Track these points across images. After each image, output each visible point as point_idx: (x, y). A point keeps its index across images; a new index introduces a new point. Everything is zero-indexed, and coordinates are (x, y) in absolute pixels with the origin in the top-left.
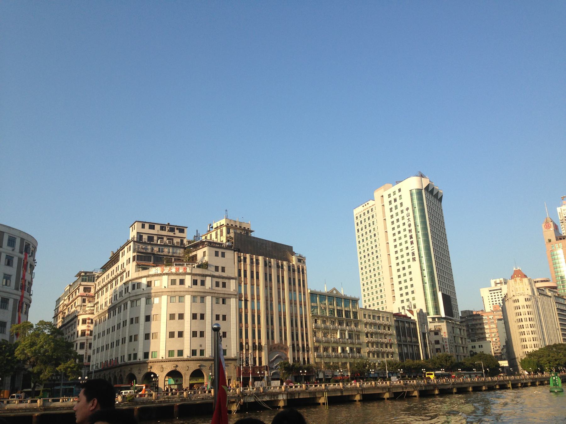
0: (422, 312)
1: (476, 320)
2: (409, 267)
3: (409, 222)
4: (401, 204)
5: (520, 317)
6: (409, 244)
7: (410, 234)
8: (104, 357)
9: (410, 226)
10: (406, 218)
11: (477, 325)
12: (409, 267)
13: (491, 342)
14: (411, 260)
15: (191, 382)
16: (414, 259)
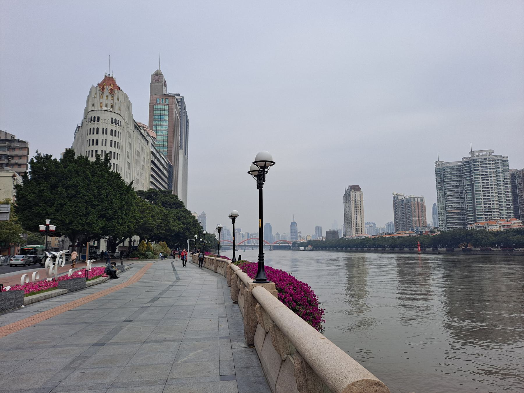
1: (14, 149)
11: (13, 157)
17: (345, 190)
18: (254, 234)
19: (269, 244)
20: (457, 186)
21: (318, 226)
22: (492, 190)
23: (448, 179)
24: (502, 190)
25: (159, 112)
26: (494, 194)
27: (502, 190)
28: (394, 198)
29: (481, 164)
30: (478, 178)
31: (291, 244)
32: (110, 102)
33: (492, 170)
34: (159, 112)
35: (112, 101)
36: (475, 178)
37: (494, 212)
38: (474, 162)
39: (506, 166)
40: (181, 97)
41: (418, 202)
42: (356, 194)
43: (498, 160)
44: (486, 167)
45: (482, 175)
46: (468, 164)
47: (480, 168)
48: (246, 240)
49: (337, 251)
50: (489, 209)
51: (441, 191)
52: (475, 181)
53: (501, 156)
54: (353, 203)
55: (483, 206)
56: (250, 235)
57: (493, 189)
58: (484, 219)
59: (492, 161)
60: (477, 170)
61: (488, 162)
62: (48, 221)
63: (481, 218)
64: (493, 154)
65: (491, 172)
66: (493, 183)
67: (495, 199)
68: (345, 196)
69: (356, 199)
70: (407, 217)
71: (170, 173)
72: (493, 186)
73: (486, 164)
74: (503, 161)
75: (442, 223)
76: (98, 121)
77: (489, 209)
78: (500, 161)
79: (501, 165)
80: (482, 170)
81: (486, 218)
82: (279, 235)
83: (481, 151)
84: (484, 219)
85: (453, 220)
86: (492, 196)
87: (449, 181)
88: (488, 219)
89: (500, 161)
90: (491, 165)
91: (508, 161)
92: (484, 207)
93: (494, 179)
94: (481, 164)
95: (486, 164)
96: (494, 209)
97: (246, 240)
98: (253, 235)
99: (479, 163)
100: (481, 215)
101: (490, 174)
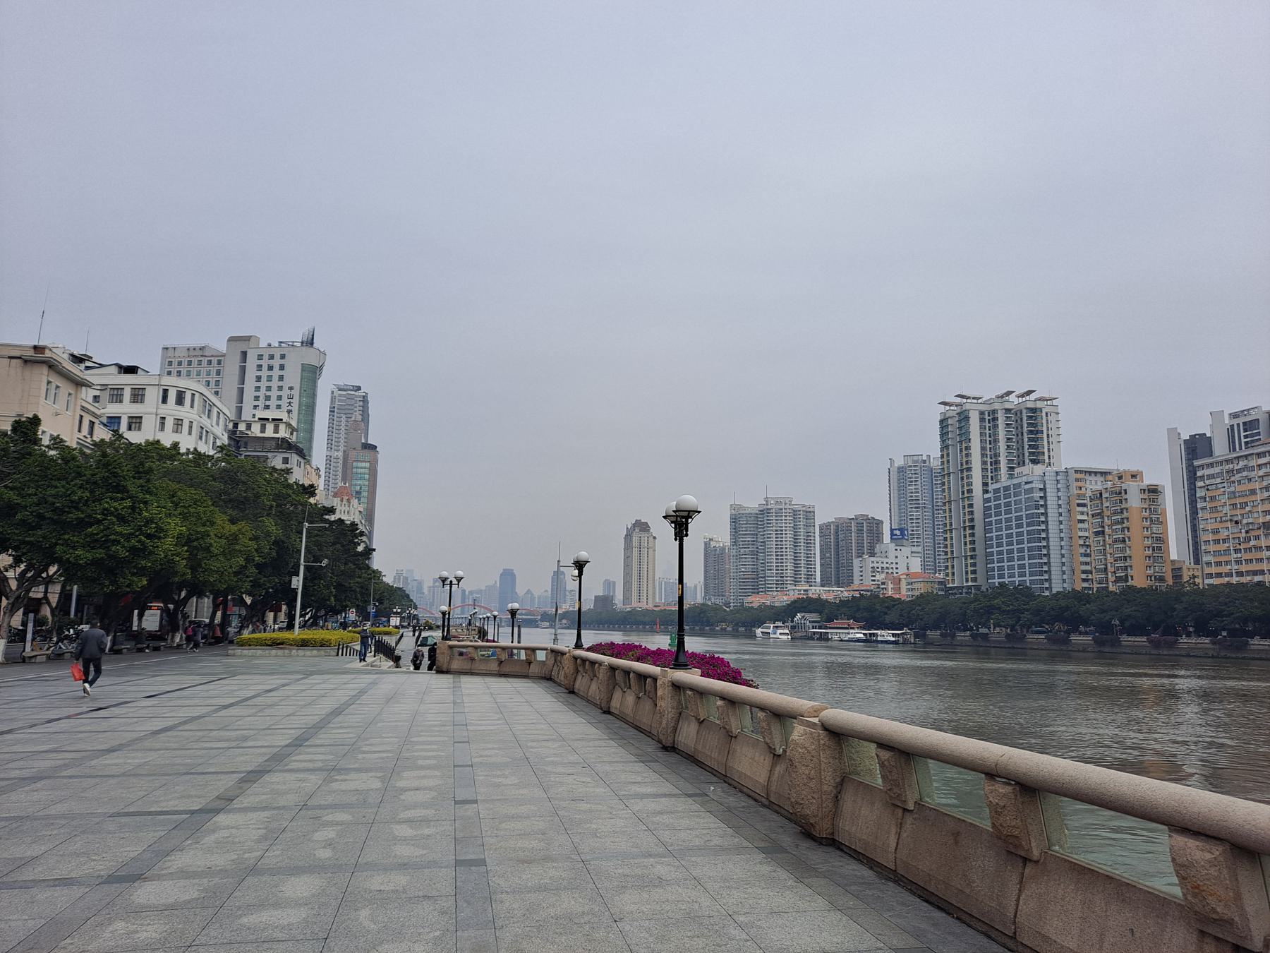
4: (281, 378)
17: (627, 528)
18: (477, 593)
19: (432, 614)
20: (753, 541)
21: (608, 580)
22: (786, 552)
23: (750, 531)
24: (802, 551)
25: (359, 470)
26: (788, 557)
27: (802, 551)
28: (705, 543)
29: (776, 516)
30: (770, 534)
31: (539, 617)
32: (347, 509)
33: (788, 525)
34: (359, 470)
36: (768, 534)
37: (787, 580)
38: (769, 513)
40: (364, 394)
42: (640, 537)
43: (799, 511)
44: (782, 520)
45: (776, 531)
47: (774, 521)
48: (457, 607)
49: (928, 660)
50: (781, 577)
51: (735, 547)
52: (768, 538)
53: (804, 506)
54: (635, 551)
56: (467, 593)
57: (788, 550)
58: (775, 589)
59: (790, 513)
60: (770, 524)
61: (784, 514)
62: (397, 607)
63: (771, 588)
65: (786, 527)
66: (788, 543)
67: (789, 564)
69: (640, 545)
70: (720, 577)
72: (788, 546)
73: (782, 516)
74: (807, 512)
75: (734, 593)
77: (781, 577)
78: (801, 513)
79: (804, 518)
80: (777, 523)
81: (777, 588)
82: (532, 594)
84: (775, 589)
85: (745, 589)
86: (786, 559)
88: (779, 589)
89: (801, 513)
90: (788, 518)
92: (776, 574)
93: (790, 537)
94: (776, 516)
95: (782, 516)
97: (457, 607)
98: (475, 595)
99: (774, 514)
100: (771, 584)
101: (786, 530)
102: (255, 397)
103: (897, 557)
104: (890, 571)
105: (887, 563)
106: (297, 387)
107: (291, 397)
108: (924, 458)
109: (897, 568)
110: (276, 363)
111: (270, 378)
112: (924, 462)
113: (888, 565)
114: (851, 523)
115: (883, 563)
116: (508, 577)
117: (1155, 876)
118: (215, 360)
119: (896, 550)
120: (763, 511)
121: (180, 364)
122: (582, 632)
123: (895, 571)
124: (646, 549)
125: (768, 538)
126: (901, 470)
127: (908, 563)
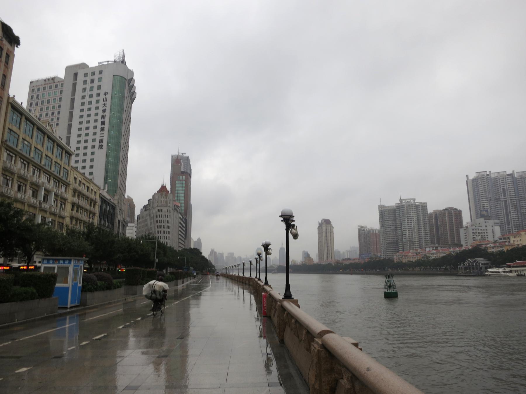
0: (292, 222)
2: (93, 153)
3: (105, 108)
4: (99, 87)
5: (160, 224)
6: (98, 130)
7: (103, 120)
8: (210, 282)
9: (104, 111)
10: (102, 102)
12: (93, 153)
13: (107, 227)
14: (97, 147)
15: (76, 82)
16: (101, 147)
23: (387, 219)
28: (359, 229)
30: (405, 219)
33: (414, 213)
35: (166, 199)
36: (403, 219)
37: (415, 244)
39: (426, 210)
41: (376, 233)
45: (408, 217)
46: (399, 209)
52: (403, 221)
55: (408, 239)
64: (415, 201)
68: (318, 228)
71: (186, 229)
76: (162, 211)
83: (407, 199)
87: (387, 220)
90: (414, 209)
91: (427, 206)
96: (415, 242)
99: (405, 208)
101: (413, 216)
102: (82, 103)
103: (486, 226)
104: (483, 234)
105: (481, 230)
106: (110, 92)
107: (105, 100)
108: (488, 173)
109: (487, 235)
110: (96, 77)
111: (91, 89)
112: (488, 175)
113: (482, 231)
114: (445, 212)
115: (479, 230)
116: (282, 221)
117: (520, 369)
118: (59, 85)
119: (485, 222)
120: (399, 207)
121: (39, 90)
122: (260, 274)
123: (486, 234)
124: (330, 233)
125: (403, 221)
126: (474, 180)
127: (493, 230)
